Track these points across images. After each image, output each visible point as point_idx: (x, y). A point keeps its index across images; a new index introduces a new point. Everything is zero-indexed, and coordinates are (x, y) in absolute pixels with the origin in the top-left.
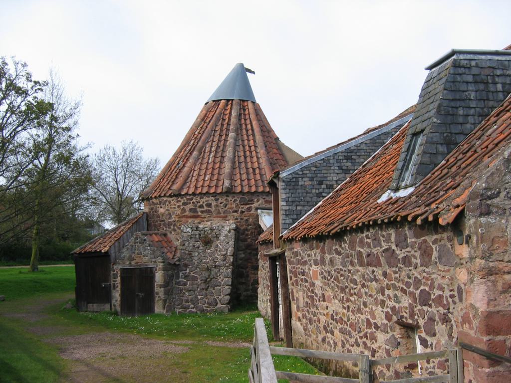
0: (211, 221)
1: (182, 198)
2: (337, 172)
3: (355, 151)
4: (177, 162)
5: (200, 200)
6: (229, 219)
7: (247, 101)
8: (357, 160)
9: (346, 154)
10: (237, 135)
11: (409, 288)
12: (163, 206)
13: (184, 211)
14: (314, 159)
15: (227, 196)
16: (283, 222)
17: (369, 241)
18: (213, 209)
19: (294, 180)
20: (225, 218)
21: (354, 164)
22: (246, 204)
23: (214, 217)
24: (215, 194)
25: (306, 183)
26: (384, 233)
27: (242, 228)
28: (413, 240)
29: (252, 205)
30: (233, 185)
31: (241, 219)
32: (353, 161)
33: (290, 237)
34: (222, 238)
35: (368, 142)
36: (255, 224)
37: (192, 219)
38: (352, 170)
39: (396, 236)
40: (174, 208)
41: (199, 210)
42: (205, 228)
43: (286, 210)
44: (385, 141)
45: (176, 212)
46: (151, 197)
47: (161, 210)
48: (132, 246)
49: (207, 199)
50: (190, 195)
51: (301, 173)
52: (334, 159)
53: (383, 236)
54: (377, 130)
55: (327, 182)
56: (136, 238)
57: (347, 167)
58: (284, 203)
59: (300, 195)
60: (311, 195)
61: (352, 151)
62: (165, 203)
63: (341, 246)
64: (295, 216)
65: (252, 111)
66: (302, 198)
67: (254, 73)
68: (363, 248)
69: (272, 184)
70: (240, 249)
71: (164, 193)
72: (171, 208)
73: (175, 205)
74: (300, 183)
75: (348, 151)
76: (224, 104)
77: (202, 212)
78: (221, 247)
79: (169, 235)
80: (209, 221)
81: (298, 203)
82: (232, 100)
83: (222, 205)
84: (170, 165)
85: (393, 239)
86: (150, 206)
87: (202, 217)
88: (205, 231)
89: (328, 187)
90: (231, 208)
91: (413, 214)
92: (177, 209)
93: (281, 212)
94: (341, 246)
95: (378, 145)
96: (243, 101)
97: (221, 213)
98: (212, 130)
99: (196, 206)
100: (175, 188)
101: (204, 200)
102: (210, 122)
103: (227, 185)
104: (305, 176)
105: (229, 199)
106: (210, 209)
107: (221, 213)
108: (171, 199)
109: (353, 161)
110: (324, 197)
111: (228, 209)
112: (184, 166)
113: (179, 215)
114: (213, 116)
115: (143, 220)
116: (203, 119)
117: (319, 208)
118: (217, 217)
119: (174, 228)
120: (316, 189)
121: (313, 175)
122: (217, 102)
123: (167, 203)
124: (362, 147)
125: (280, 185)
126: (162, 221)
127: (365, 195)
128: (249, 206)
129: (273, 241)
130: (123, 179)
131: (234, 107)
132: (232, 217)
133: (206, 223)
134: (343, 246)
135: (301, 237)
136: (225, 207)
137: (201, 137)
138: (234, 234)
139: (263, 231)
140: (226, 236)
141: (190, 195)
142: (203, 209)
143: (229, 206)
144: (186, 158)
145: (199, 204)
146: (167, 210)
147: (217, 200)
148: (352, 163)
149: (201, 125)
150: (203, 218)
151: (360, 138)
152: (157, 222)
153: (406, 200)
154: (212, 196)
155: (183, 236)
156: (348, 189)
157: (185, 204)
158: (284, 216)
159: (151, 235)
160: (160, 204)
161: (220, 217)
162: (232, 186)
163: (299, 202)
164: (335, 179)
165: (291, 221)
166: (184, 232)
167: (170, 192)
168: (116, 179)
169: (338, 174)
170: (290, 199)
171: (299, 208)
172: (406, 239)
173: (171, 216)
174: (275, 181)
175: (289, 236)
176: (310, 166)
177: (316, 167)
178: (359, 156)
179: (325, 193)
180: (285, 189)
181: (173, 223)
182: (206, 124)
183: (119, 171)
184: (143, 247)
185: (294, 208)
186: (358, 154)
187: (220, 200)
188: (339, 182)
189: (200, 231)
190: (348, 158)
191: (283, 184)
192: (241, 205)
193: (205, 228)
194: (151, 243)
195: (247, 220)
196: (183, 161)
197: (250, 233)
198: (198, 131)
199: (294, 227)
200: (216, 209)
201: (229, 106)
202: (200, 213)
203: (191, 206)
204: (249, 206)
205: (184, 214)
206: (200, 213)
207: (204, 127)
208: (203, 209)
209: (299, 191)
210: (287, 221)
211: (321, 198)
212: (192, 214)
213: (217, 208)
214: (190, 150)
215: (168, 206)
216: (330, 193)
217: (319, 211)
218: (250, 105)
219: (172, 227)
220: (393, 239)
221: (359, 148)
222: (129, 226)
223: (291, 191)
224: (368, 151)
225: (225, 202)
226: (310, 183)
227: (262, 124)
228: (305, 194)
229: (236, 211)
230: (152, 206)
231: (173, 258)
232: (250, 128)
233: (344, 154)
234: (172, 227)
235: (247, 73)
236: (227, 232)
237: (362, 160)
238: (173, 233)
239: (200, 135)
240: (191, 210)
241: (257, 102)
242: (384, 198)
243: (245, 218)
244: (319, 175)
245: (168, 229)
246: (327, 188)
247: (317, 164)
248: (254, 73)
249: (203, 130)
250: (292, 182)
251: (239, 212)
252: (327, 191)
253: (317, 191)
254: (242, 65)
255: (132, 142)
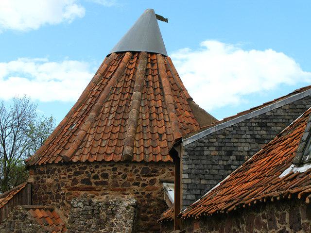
0: (106, 195)
1: (74, 167)
2: (249, 141)
3: (271, 117)
4: (70, 123)
7: (156, 54)
8: (273, 128)
9: (260, 121)
10: (142, 94)
11: (93, 178)
12: (51, 176)
13: (75, 181)
14: (222, 126)
15: (127, 166)
16: (184, 197)
17: (265, 221)
18: (110, 181)
19: (199, 149)
20: (123, 192)
21: (269, 131)
22: (149, 176)
23: (111, 190)
24: (112, 163)
25: (213, 153)
26: (279, 213)
27: (144, 204)
28: (306, 221)
30: (134, 152)
32: (269, 129)
33: (189, 216)
34: (118, 215)
35: (286, 108)
36: (159, 200)
37: (84, 192)
38: (267, 139)
39: (290, 216)
40: (64, 178)
41: (92, 181)
42: (99, 202)
43: (188, 184)
44: (307, 106)
45: (65, 183)
46: (38, 164)
47: (49, 181)
48: (11, 222)
49: (104, 168)
50: (84, 163)
51: (207, 141)
52: (246, 126)
53: (278, 216)
54: (298, 94)
55: (237, 152)
56: (16, 213)
57: (262, 135)
58: (186, 176)
59: (206, 166)
60: (218, 167)
61: (267, 118)
62: (53, 172)
63: (239, 227)
64: (199, 191)
65: (162, 66)
66: (208, 171)
67: (166, 20)
68: (259, 230)
69: (174, 153)
70: (141, 229)
71: (52, 160)
72: (60, 178)
73: (66, 175)
74: (206, 153)
75: (263, 117)
76: (129, 57)
77: (96, 183)
78: (117, 226)
79: (56, 210)
80: (105, 194)
81: (202, 176)
82: (139, 53)
83: (120, 176)
84: (62, 126)
85: (287, 220)
86: (36, 174)
89: (239, 157)
90: (131, 180)
91: (302, 192)
92: (67, 179)
93: (182, 186)
94: (239, 227)
95: (299, 110)
96: (152, 54)
97: (118, 186)
98: (113, 88)
99: (89, 176)
100: (65, 155)
101: (99, 169)
102: (111, 77)
103: (127, 153)
104: (210, 144)
105: (130, 168)
106: (106, 180)
108: (60, 168)
109: (269, 129)
110: (233, 170)
111: (128, 180)
112: (78, 128)
114: (115, 71)
115: (26, 192)
116: (103, 74)
117: (225, 182)
119: (63, 202)
120: (223, 160)
121: (220, 144)
122: (120, 54)
123: (56, 172)
124: (279, 112)
125: (183, 155)
126: (49, 193)
127: (271, 169)
128: (152, 178)
129: (173, 220)
130: (13, 141)
131: (141, 61)
132: (132, 190)
133: (101, 197)
134: (241, 227)
135: (199, 216)
136: (124, 179)
137: (99, 95)
138: (133, 210)
139: (168, 207)
140: (124, 212)
142: (98, 181)
143: (128, 177)
144: (82, 119)
145: (93, 175)
146: (56, 180)
147: (114, 170)
148: (266, 131)
149: (101, 81)
150: (97, 191)
151: (277, 102)
152: (43, 194)
153: (304, 176)
154: (109, 166)
155: (73, 212)
156: (259, 161)
157: (76, 174)
158: (186, 191)
159: (34, 209)
160: (47, 173)
161: (118, 190)
162: (133, 154)
163: (204, 175)
164: (246, 149)
165: (194, 197)
166: (74, 208)
167: (60, 159)
168: (4, 142)
169: (250, 143)
170: (193, 171)
171: (203, 182)
172: (299, 220)
173: (59, 188)
174: (177, 149)
175: (188, 215)
176: (218, 133)
177: (224, 134)
178: (276, 123)
179: (235, 165)
180: (187, 159)
181: (62, 196)
182: (106, 80)
183: (8, 130)
184: (24, 224)
185: (198, 182)
186: (275, 121)
187: (118, 171)
188: (252, 153)
189: (93, 206)
190: (262, 125)
191: (186, 153)
192: (143, 176)
194: (33, 219)
196: (77, 123)
197: (152, 210)
198: (97, 88)
199: (195, 204)
200: (114, 181)
201: (135, 60)
203: (84, 176)
204: (152, 178)
205: (75, 186)
206: (94, 185)
207: (103, 83)
208: (98, 181)
209: (204, 162)
210: (189, 197)
211: (230, 171)
212: (85, 186)
213: (115, 179)
214: (86, 110)
215: (56, 175)
216: (240, 165)
217: (224, 185)
218: (160, 60)
219: (61, 201)
220: (287, 220)
221: (275, 114)
222: (9, 199)
223: (194, 162)
224: (286, 117)
225: (124, 173)
226: (217, 153)
227: (172, 82)
228: (211, 166)
229: (137, 184)
230: (38, 175)
232: (158, 86)
233: (258, 121)
234: (61, 201)
235: (158, 21)
237: (280, 128)
238: (61, 208)
239: (99, 93)
240: (83, 181)
241: (169, 56)
242: (286, 172)
243: (147, 193)
244: (227, 144)
245: (55, 203)
246: (237, 159)
247: (226, 132)
248: (166, 20)
249: (103, 86)
250: (196, 152)
251: (140, 185)
252: (236, 163)
253: (225, 163)
254: (152, 11)
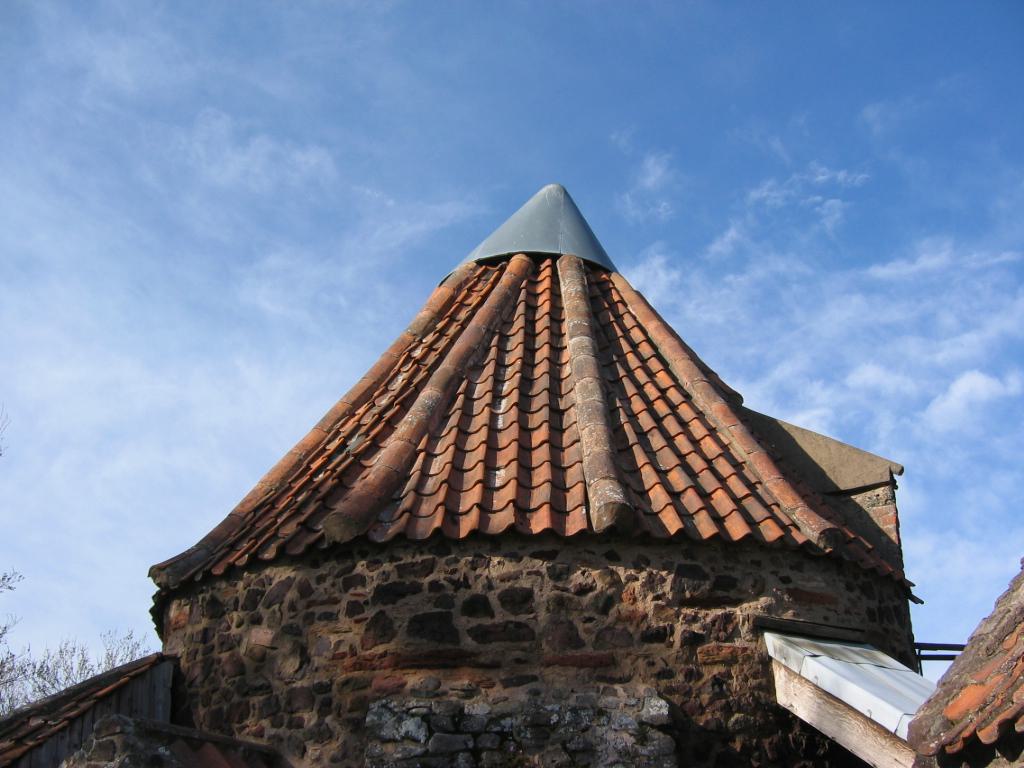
5: (472, 575)
6: (627, 672)
23: (548, 665)
29: (737, 611)
31: (691, 675)
41: (463, 623)
42: (503, 716)
50: (421, 545)
77: (482, 635)
80: (520, 681)
87: (482, 660)
88: (504, 736)
92: (344, 622)
99: (447, 602)
102: (469, 319)
107: (580, 644)
113: (353, 651)
118: (563, 662)
119: (319, 724)
132: (641, 663)
141: (421, 545)
142: (487, 621)
145: (463, 595)
154: (534, 556)
161: (580, 663)
189: (476, 735)
193: (503, 716)
195: (718, 681)
202: (468, 643)
206: (468, 643)
208: (487, 621)
231: (714, 712)
236: (630, 740)
240: (419, 625)
255: (130, 637)
